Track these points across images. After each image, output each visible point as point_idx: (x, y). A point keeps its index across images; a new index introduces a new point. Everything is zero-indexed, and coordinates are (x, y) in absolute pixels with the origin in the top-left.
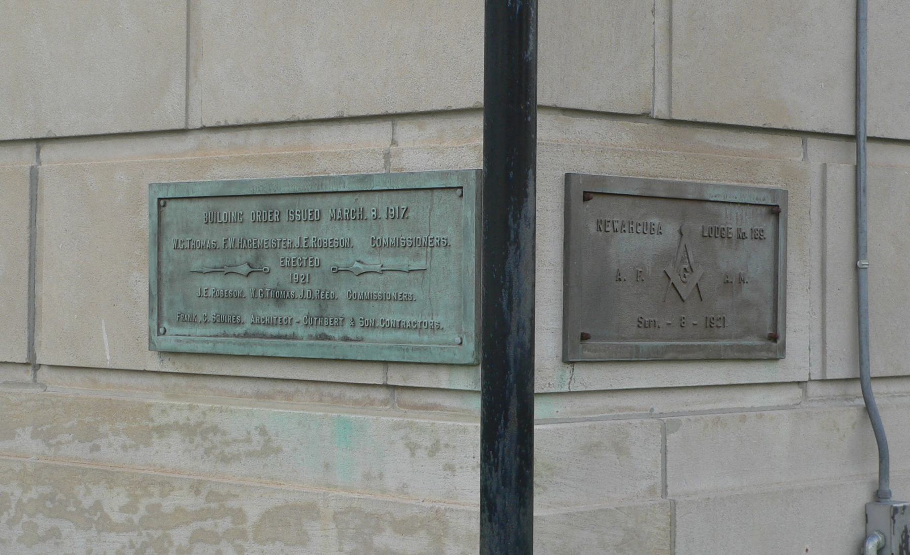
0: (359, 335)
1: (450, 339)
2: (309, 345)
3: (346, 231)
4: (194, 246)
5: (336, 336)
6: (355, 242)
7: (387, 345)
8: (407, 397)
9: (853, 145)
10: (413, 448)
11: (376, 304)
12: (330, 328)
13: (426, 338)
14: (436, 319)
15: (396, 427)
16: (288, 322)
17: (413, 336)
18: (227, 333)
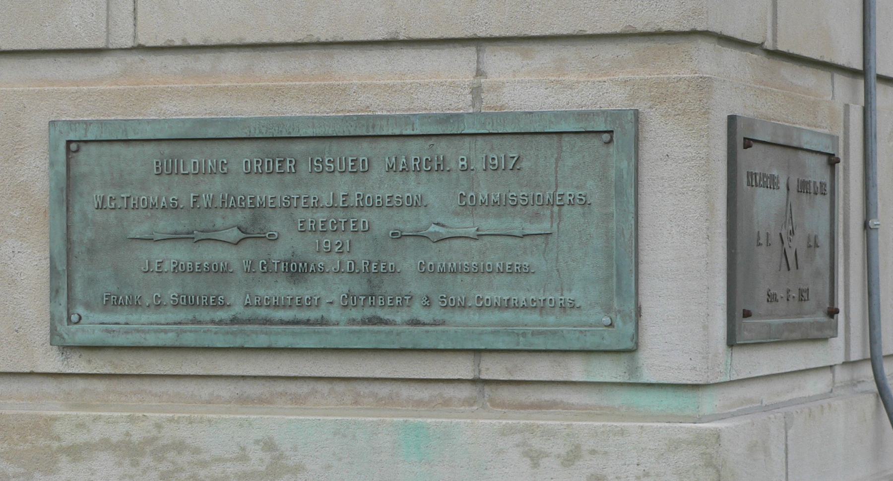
0: (438, 318)
1: (592, 320)
2: (353, 332)
3: (413, 186)
4: (132, 205)
5: (398, 319)
6: (431, 199)
7: (489, 329)
8: (506, 394)
9: (861, 83)
10: (535, 458)
11: (467, 278)
12: (386, 310)
13: (551, 319)
14: (568, 296)
15: (505, 432)
16: (311, 303)
17: (533, 317)
18: (199, 318)
